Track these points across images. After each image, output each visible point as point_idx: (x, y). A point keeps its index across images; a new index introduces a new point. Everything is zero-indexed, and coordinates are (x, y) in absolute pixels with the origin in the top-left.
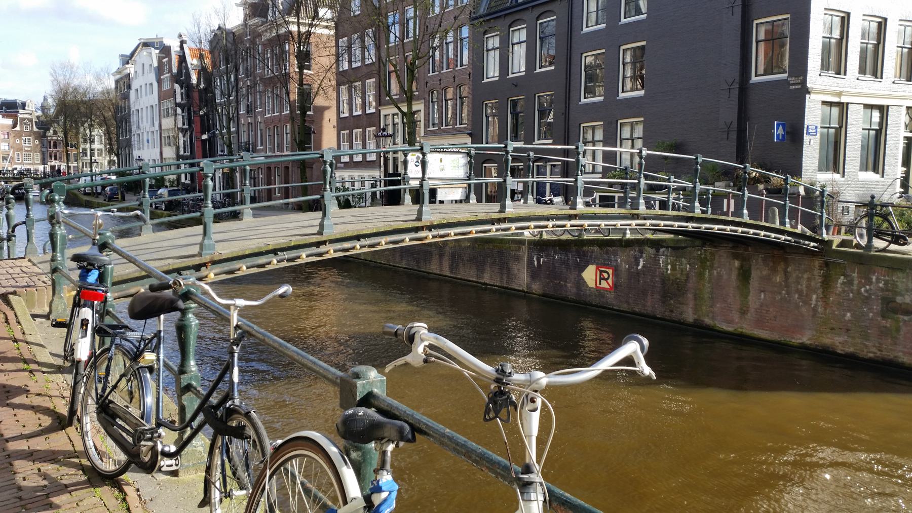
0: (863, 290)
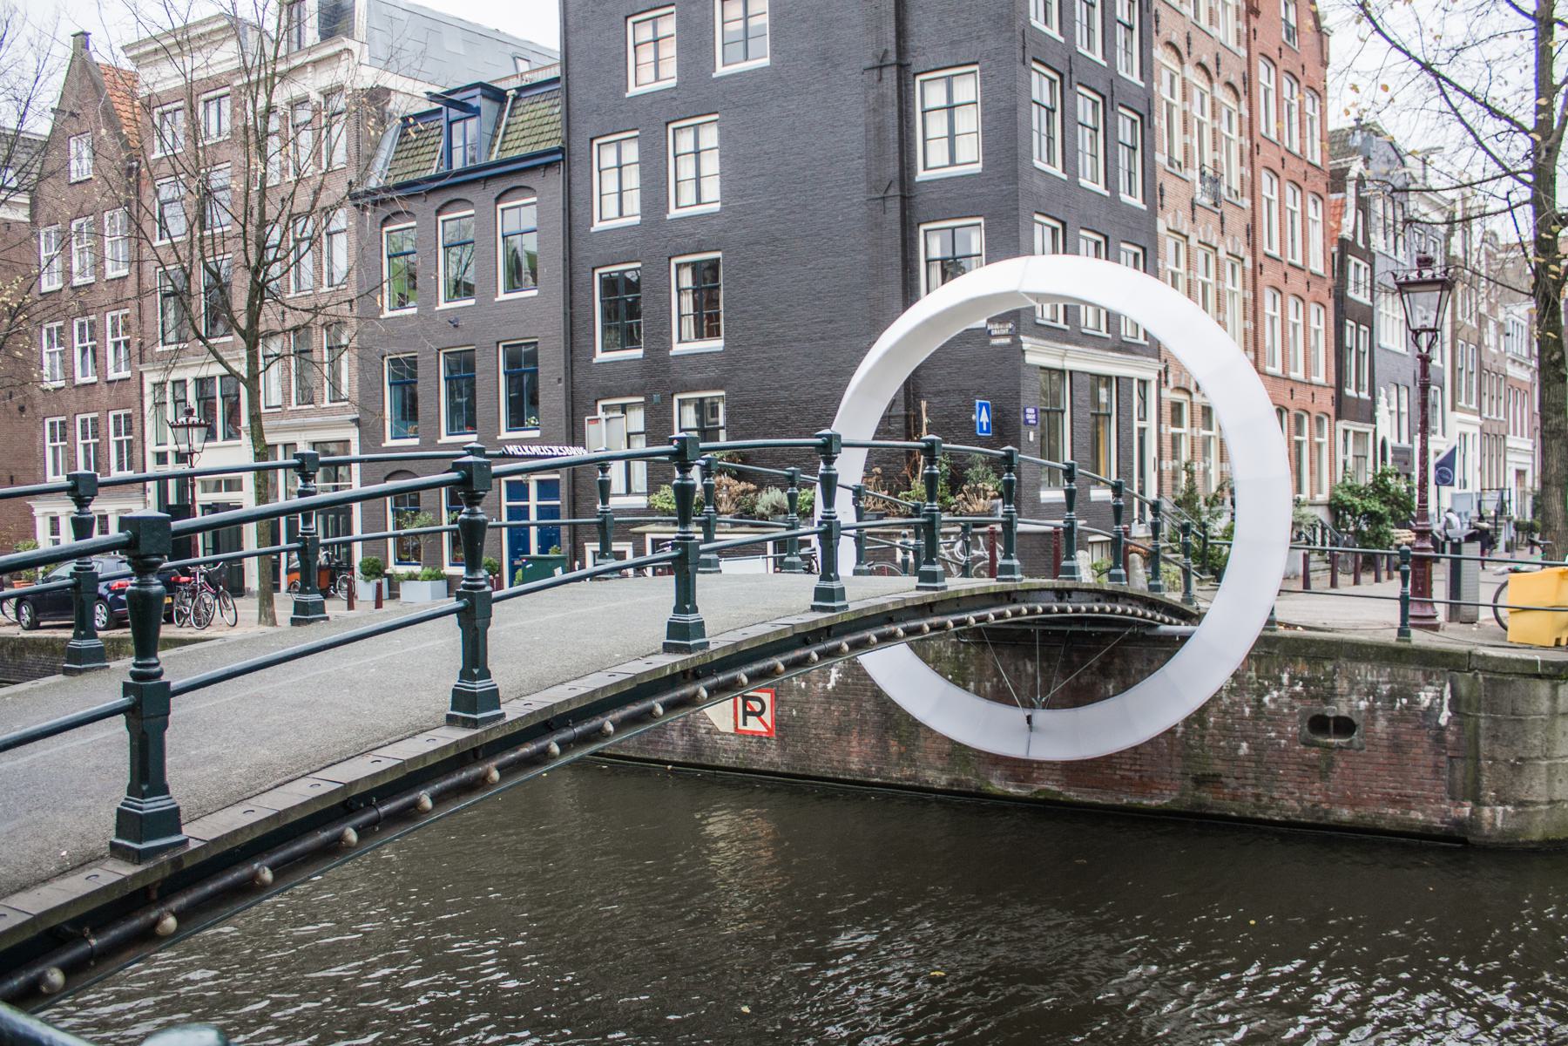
0: (1266, 699)
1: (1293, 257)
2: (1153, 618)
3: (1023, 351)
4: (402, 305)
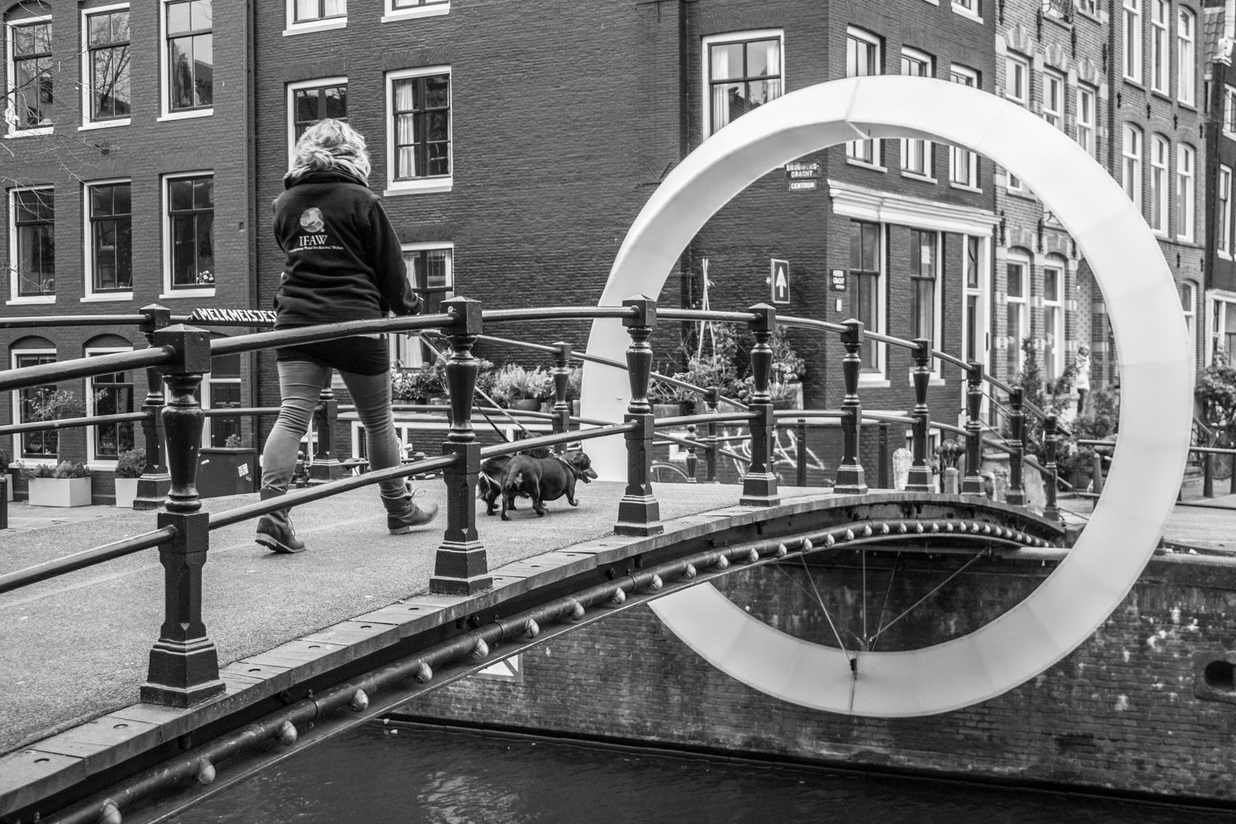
0: (1151, 640)
1: (1158, 86)
2: (1013, 538)
3: (831, 198)
4: (33, 123)
